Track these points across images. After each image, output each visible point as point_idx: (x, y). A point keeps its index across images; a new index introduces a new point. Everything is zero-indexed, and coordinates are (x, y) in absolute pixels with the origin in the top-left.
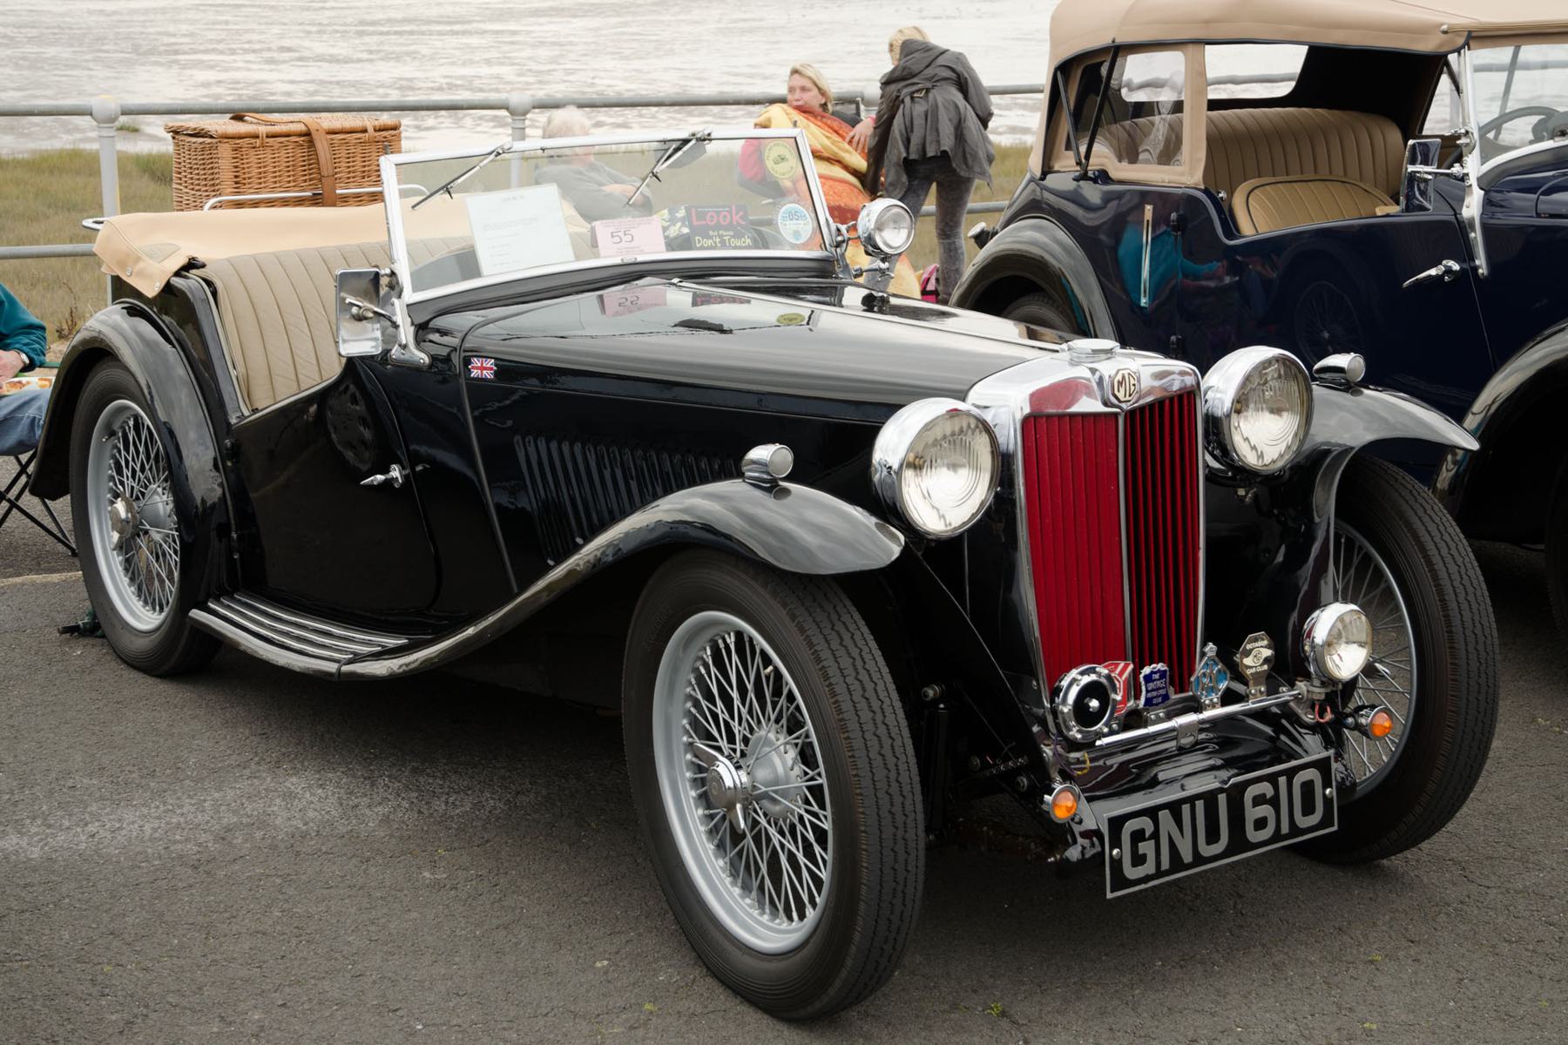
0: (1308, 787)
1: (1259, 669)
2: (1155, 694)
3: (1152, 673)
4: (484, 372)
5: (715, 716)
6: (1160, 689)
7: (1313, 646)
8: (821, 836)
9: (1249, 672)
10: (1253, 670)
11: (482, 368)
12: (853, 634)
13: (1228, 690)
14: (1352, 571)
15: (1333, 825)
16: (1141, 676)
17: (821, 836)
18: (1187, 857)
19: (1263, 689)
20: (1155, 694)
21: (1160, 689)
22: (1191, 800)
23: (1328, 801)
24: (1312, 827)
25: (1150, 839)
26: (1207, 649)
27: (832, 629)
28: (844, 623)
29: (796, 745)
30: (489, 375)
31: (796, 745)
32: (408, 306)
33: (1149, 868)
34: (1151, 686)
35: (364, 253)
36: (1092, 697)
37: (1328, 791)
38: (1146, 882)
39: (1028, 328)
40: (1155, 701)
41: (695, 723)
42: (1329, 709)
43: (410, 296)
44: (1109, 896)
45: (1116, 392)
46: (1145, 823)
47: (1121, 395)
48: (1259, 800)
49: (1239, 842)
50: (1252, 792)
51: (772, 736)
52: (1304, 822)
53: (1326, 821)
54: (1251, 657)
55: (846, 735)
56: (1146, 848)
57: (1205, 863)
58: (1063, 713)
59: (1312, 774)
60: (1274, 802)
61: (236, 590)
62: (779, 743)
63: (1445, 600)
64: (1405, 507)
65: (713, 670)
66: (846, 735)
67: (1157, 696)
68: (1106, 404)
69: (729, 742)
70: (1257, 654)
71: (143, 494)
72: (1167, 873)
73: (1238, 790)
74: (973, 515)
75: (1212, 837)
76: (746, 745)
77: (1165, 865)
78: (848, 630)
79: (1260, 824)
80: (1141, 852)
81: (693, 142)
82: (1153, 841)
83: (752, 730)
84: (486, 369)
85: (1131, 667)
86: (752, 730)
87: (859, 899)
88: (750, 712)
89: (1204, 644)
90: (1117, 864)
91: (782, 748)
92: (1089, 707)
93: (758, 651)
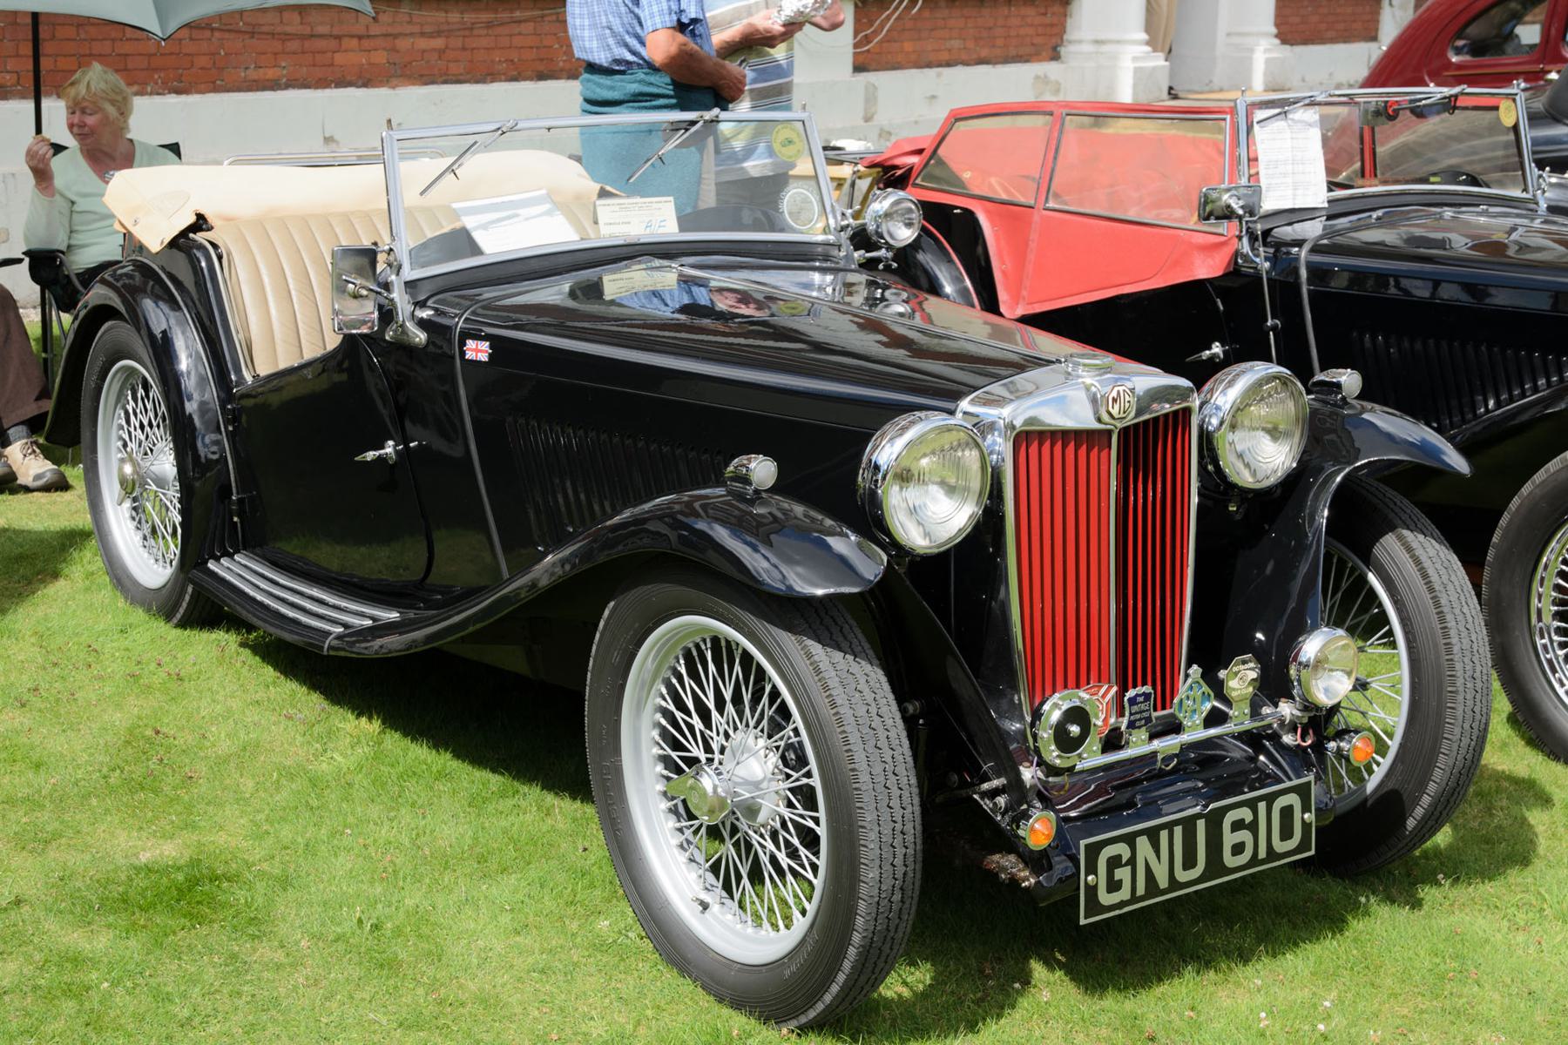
0: (1287, 812)
1: (1244, 692)
2: (1138, 716)
3: (1137, 695)
4: (479, 354)
5: (691, 728)
6: (1144, 711)
9: (1234, 694)
11: (477, 351)
12: (842, 628)
13: (1214, 709)
14: (1339, 595)
15: (1310, 850)
16: (1126, 699)
18: (1163, 883)
19: (1246, 711)
20: (1138, 716)
21: (1144, 711)
22: (1170, 826)
23: (1306, 826)
24: (1289, 852)
25: (1126, 865)
26: (1191, 671)
27: (821, 623)
28: (832, 617)
29: (777, 748)
30: (484, 357)
31: (777, 748)
32: (406, 283)
33: (1124, 894)
34: (1135, 708)
36: (1073, 723)
38: (1120, 909)
39: (476, 250)
40: (1138, 724)
41: (664, 734)
42: (1311, 732)
43: (409, 273)
44: (1083, 922)
45: (1110, 409)
46: (1122, 849)
47: (1115, 412)
48: (1238, 826)
49: (1215, 865)
51: (751, 740)
52: (1280, 846)
55: (835, 710)
56: (1123, 874)
57: (1181, 889)
58: (1042, 738)
60: (1253, 827)
61: (237, 552)
62: (758, 747)
63: (1430, 582)
64: (1391, 515)
66: (835, 710)
67: (1140, 719)
68: (1099, 420)
69: (706, 752)
70: (1241, 678)
71: (151, 450)
72: (1142, 899)
73: (1215, 820)
74: (960, 530)
75: (1189, 863)
77: (1141, 891)
78: (836, 624)
79: (1238, 849)
81: (701, 123)
82: (1129, 867)
83: (154, 445)
84: (481, 351)
89: (1189, 666)
90: (1092, 891)
91: (762, 752)
92: (1070, 732)
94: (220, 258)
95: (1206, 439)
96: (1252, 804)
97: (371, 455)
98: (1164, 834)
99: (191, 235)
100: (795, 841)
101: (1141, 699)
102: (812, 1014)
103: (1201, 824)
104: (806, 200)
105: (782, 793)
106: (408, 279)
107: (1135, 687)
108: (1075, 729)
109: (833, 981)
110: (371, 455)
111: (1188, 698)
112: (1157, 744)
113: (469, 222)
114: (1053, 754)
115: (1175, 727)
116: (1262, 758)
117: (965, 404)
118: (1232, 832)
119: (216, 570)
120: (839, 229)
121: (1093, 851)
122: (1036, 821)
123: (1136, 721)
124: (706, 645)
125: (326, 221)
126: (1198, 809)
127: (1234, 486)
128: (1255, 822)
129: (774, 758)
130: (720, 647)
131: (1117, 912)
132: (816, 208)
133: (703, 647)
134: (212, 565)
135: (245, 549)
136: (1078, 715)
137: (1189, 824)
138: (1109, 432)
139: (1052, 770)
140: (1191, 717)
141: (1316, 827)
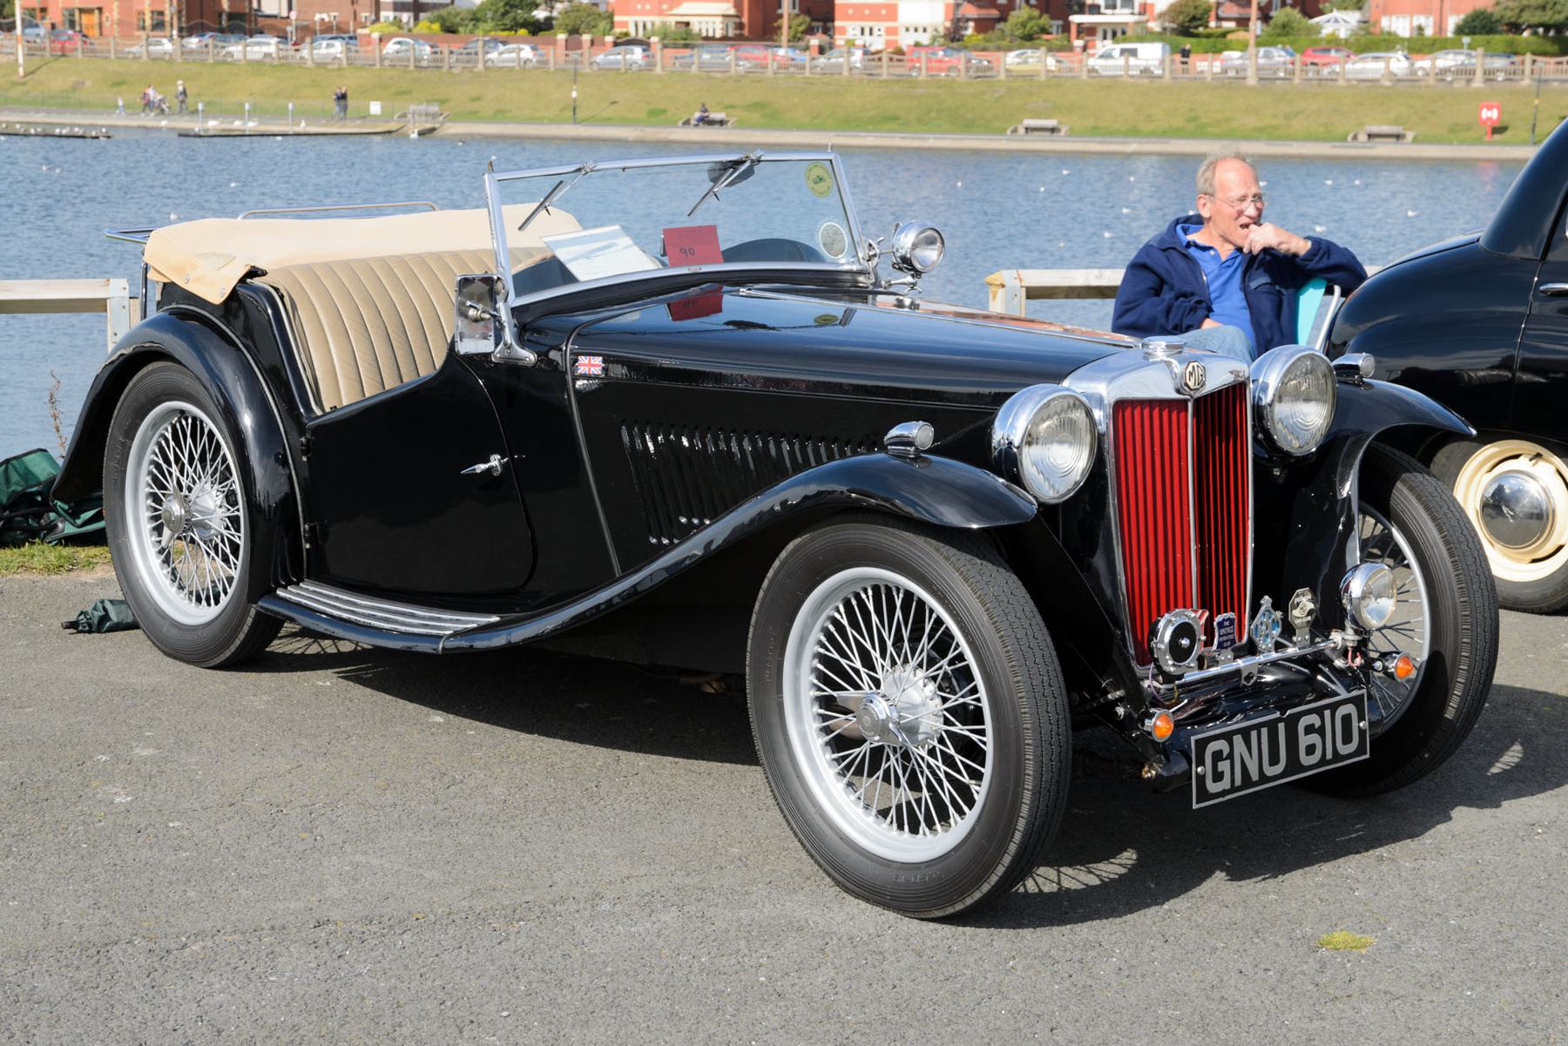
0: (1347, 719)
2: (1225, 638)
3: (1224, 620)
7: (1351, 600)
8: (235, 549)
9: (1297, 622)
10: (1300, 621)
15: (1366, 753)
16: (1215, 624)
17: (235, 549)
18: (1255, 777)
20: (1225, 638)
22: (1258, 727)
23: (1362, 732)
25: (1226, 759)
33: (1225, 784)
34: (1223, 631)
35: (475, 255)
37: (1361, 724)
39: (569, 278)
40: (1225, 645)
44: (1195, 806)
46: (1221, 745)
48: (1310, 729)
49: (1294, 765)
50: (1304, 722)
52: (1344, 750)
53: (1360, 750)
54: (1298, 609)
56: (1224, 766)
59: (1350, 709)
60: (1321, 731)
65: (172, 443)
67: (1227, 641)
70: (1304, 604)
73: (1292, 723)
75: (1274, 760)
76: (190, 492)
77: (1238, 782)
79: (1311, 750)
80: (1220, 770)
82: (1229, 761)
83: (194, 482)
84: (594, 366)
85: (1207, 614)
86: (194, 482)
87: (1022, 803)
88: (195, 471)
90: (1201, 779)
91: (921, 683)
93: (206, 432)
94: (282, 297)
95: (1259, 411)
96: (1319, 711)
97: (481, 467)
98: (1254, 734)
99: (248, 280)
100: (952, 751)
101: (1227, 623)
102: (959, 907)
103: (1281, 726)
104: (837, 232)
105: (940, 713)
106: (514, 305)
107: (1226, 611)
108: (1185, 642)
109: (1005, 852)
110: (481, 467)
111: (1262, 624)
112: (1240, 663)
113: (562, 255)
114: (1169, 665)
115: (1251, 649)
116: (1320, 678)
117: (1066, 383)
118: (1306, 734)
119: (288, 596)
120: (867, 258)
121: (1202, 744)
122: (1157, 719)
123: (1224, 642)
124: (866, 593)
125: (455, 255)
126: (1278, 714)
127: (1279, 450)
128: (1322, 729)
129: (932, 686)
130: (883, 593)
131: (1221, 800)
132: (847, 239)
133: (864, 596)
134: (280, 593)
135: (309, 578)
136: (1184, 630)
137: (1272, 726)
138: (1186, 401)
139: (1168, 678)
140: (1264, 641)
141: (1370, 736)
